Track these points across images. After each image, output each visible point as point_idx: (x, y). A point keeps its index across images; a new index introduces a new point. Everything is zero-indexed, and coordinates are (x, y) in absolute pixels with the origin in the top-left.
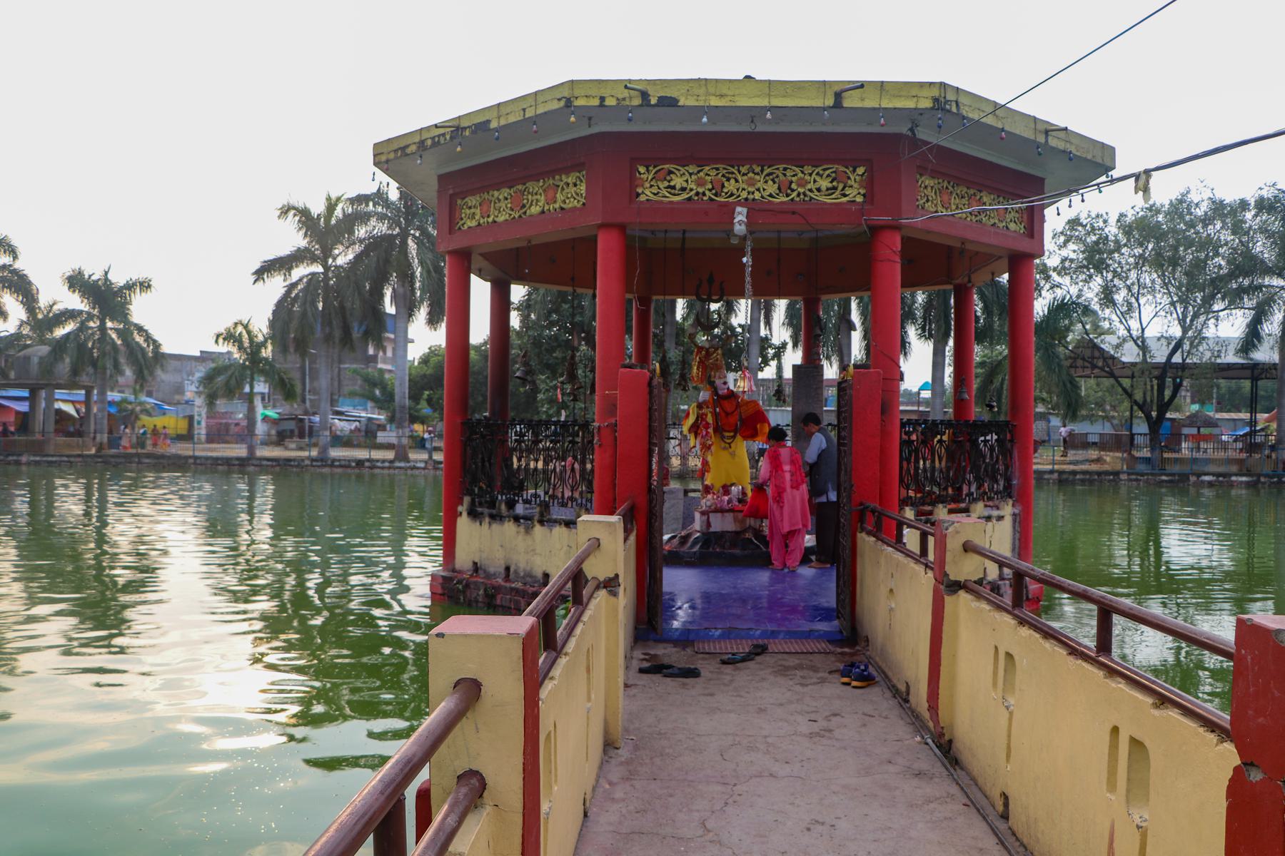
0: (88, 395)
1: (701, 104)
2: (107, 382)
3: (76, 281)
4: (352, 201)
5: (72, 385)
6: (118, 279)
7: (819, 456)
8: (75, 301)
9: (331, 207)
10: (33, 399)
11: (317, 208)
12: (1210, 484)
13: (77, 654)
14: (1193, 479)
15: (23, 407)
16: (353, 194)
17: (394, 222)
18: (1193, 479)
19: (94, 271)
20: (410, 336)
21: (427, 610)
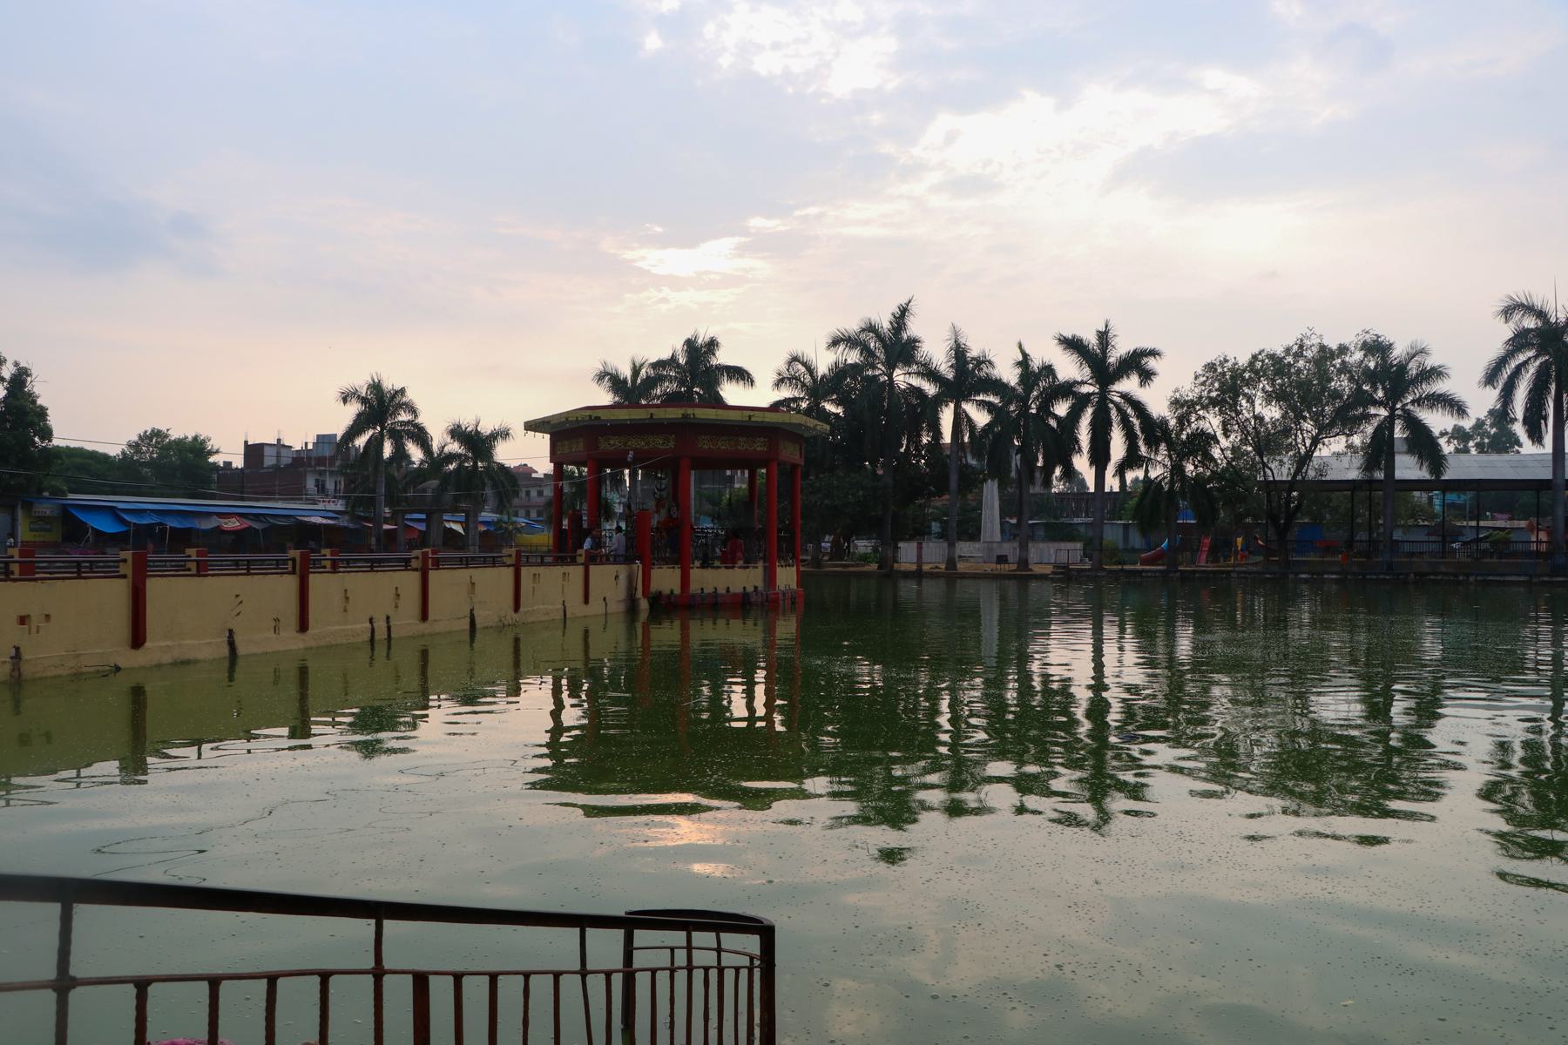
0: (467, 517)
1: (1063, 545)
2: (479, 503)
3: (457, 433)
4: (655, 365)
5: (455, 510)
6: (486, 428)
7: (1433, 369)
8: (455, 447)
9: (636, 371)
10: (427, 521)
11: (626, 372)
12: (1306, 581)
13: (394, 751)
14: (1291, 576)
15: (422, 527)
16: (653, 360)
17: (682, 383)
18: (1291, 576)
19: (467, 422)
20: (311, 415)
21: (545, 751)
